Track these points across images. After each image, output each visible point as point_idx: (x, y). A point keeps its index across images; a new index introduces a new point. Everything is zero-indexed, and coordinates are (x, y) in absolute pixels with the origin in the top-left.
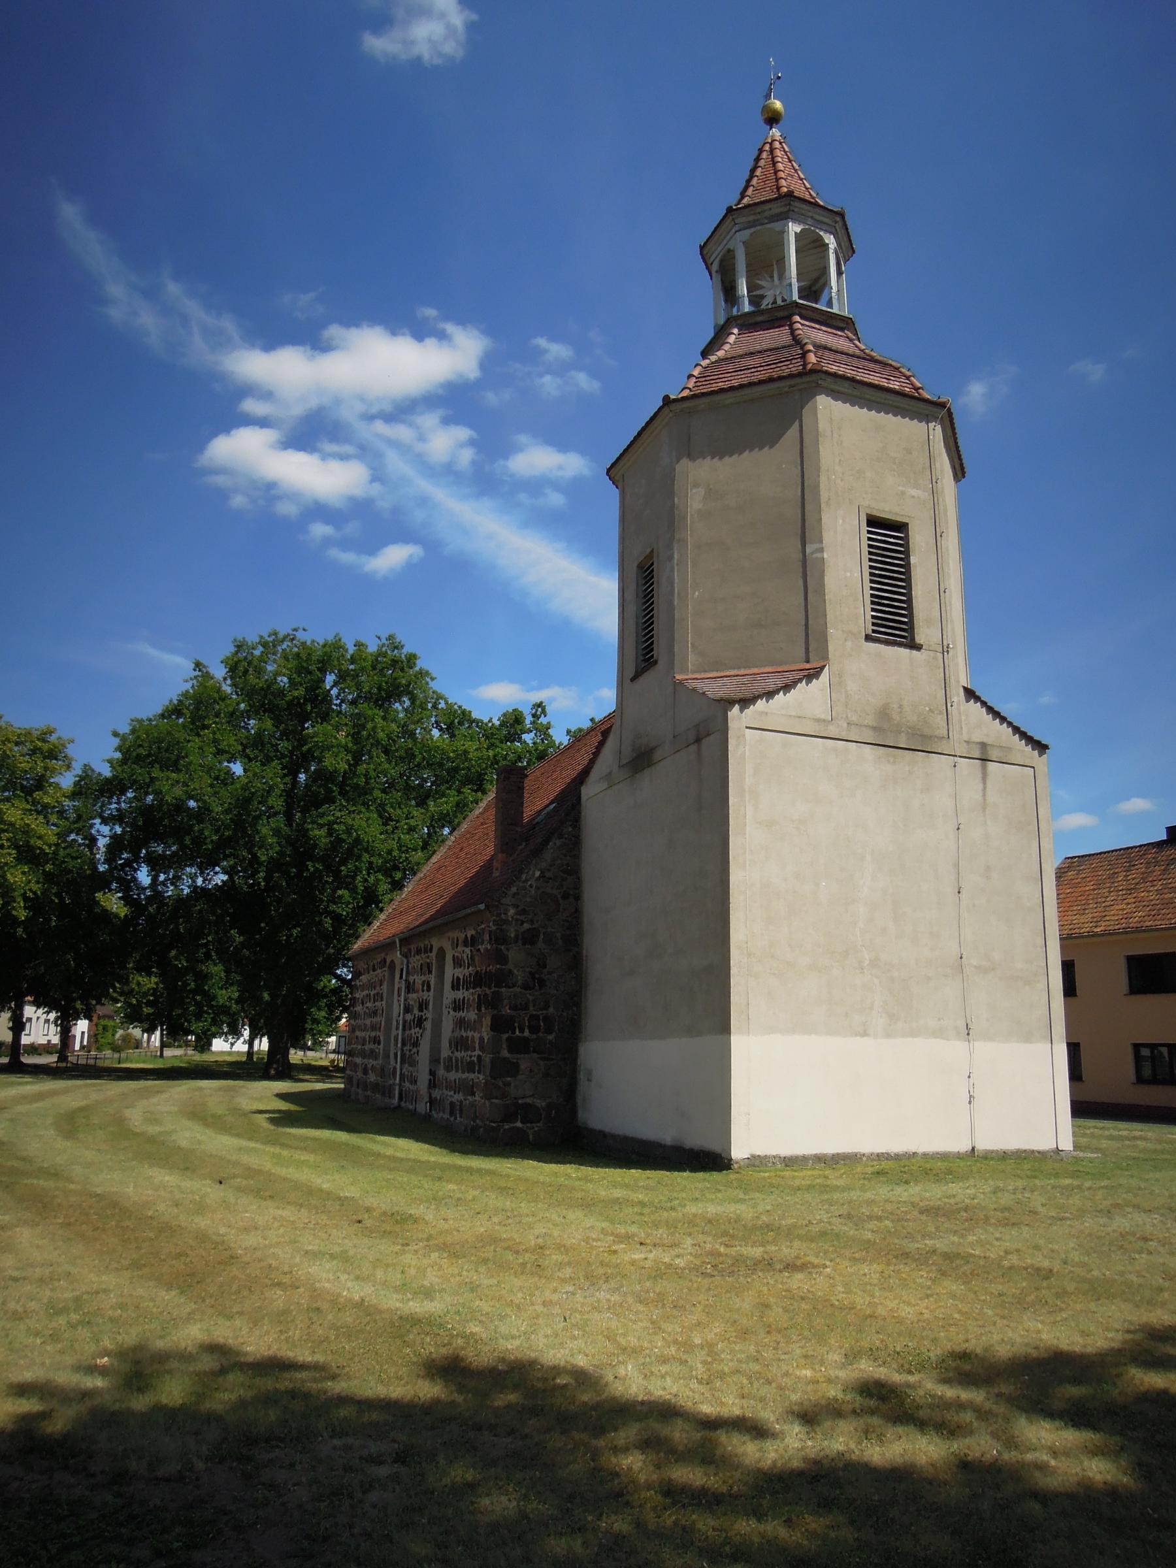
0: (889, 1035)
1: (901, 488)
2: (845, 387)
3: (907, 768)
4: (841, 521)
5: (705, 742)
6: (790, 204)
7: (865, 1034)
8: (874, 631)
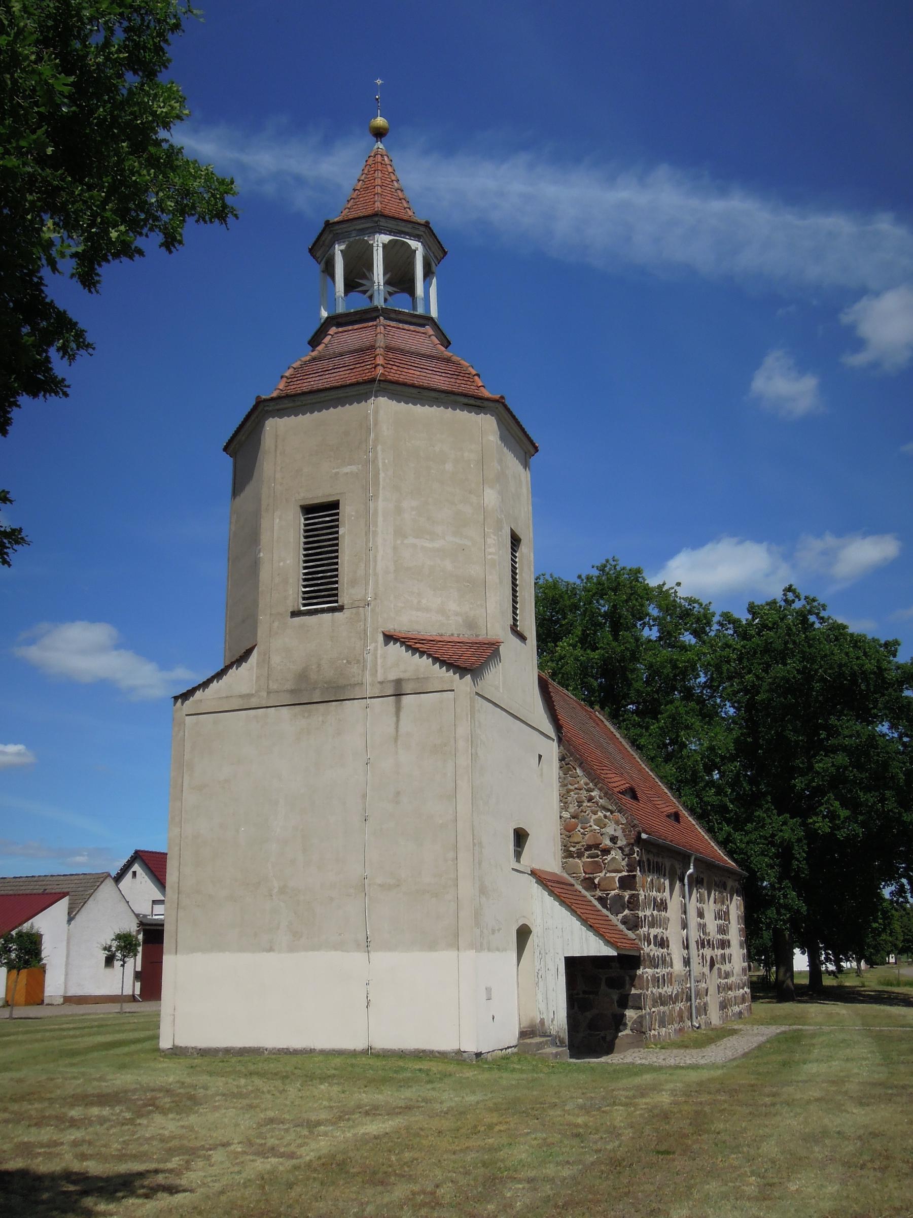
0: (291, 949)
1: (334, 471)
2: (287, 404)
3: (320, 719)
4: (278, 520)
5: (405, 700)
6: (331, 231)
7: (271, 949)
8: (305, 605)
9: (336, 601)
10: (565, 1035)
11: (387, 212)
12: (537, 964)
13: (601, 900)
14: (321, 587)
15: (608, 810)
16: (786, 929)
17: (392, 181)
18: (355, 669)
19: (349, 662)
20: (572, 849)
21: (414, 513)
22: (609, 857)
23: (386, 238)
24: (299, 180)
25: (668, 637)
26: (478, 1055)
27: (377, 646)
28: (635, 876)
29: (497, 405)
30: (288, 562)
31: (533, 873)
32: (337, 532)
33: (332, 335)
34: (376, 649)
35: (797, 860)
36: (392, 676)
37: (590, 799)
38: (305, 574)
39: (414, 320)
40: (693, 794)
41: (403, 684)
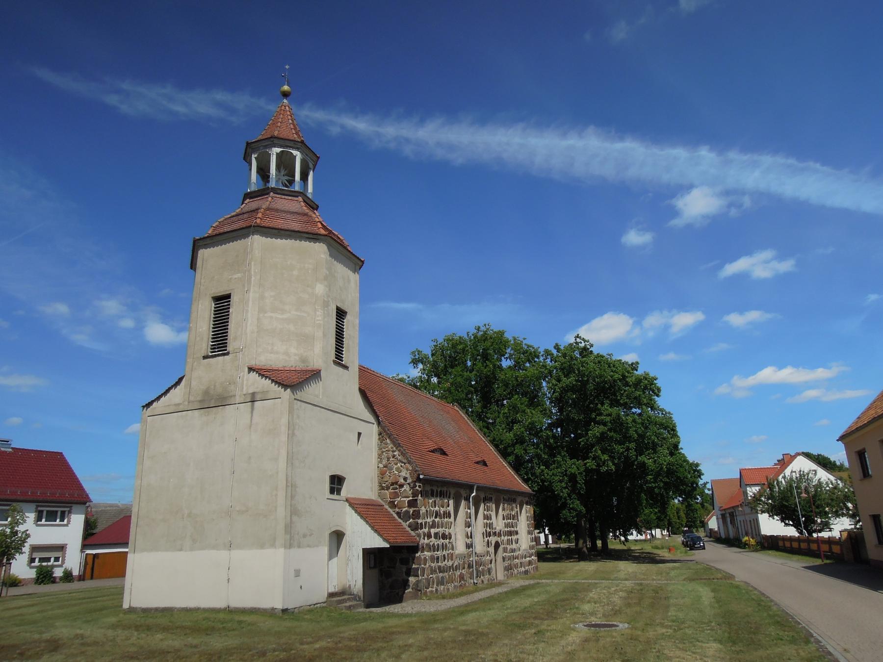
0: (192, 549)
1: (230, 277)
5: (257, 404)
7: (181, 550)
9: (226, 350)
10: (361, 594)
11: (281, 136)
12: (347, 553)
13: (398, 514)
14: (220, 342)
15: (402, 462)
16: (574, 521)
17: (289, 119)
18: (232, 387)
19: (230, 384)
20: (383, 485)
21: (272, 299)
22: (403, 489)
23: (278, 150)
24: (407, 140)
25: (518, 365)
26: (285, 611)
27: (244, 374)
28: (416, 500)
29: (326, 237)
30: (204, 329)
31: (347, 500)
32: (229, 311)
33: (246, 204)
34: (243, 376)
35: (580, 484)
36: (251, 391)
37: (394, 456)
38: (213, 335)
39: (291, 194)
40: (521, 448)
41: (256, 394)
